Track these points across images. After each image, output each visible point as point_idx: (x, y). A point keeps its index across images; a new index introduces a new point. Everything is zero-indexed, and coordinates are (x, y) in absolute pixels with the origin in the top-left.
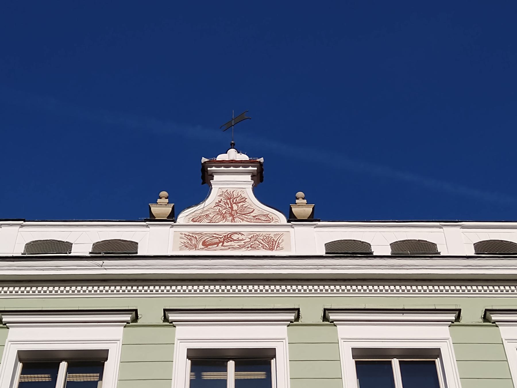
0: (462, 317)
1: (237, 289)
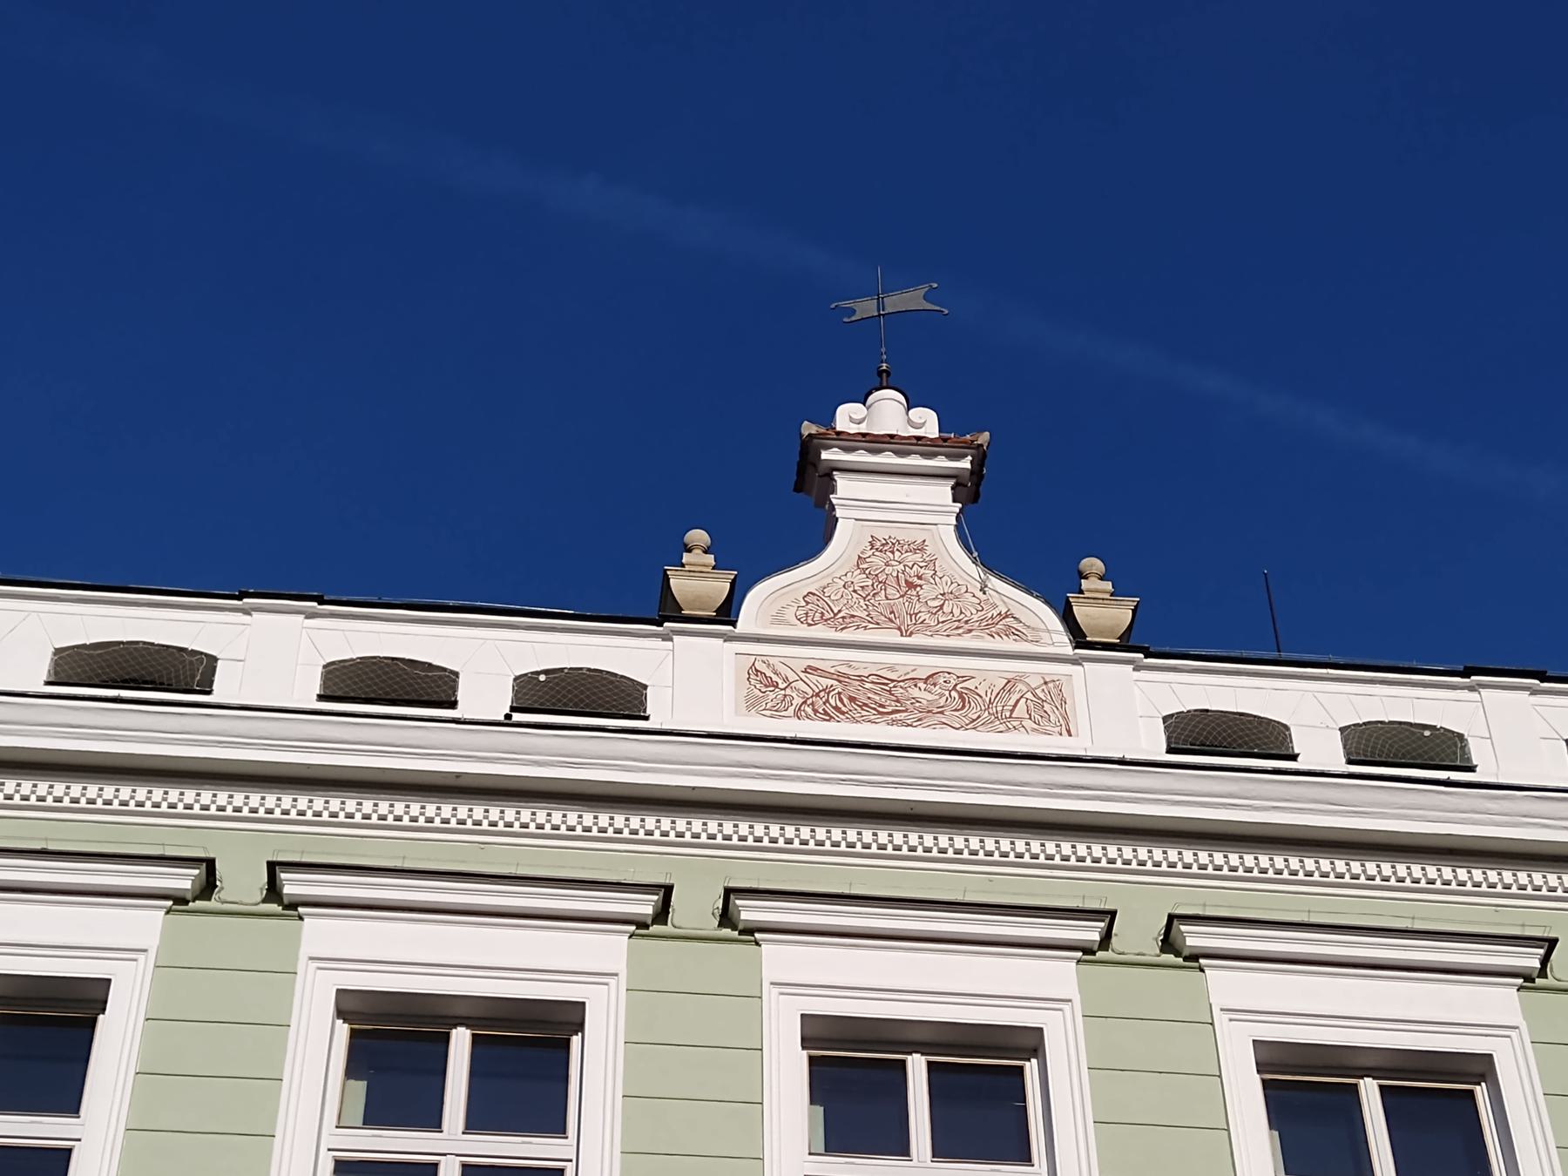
0: (673, 910)
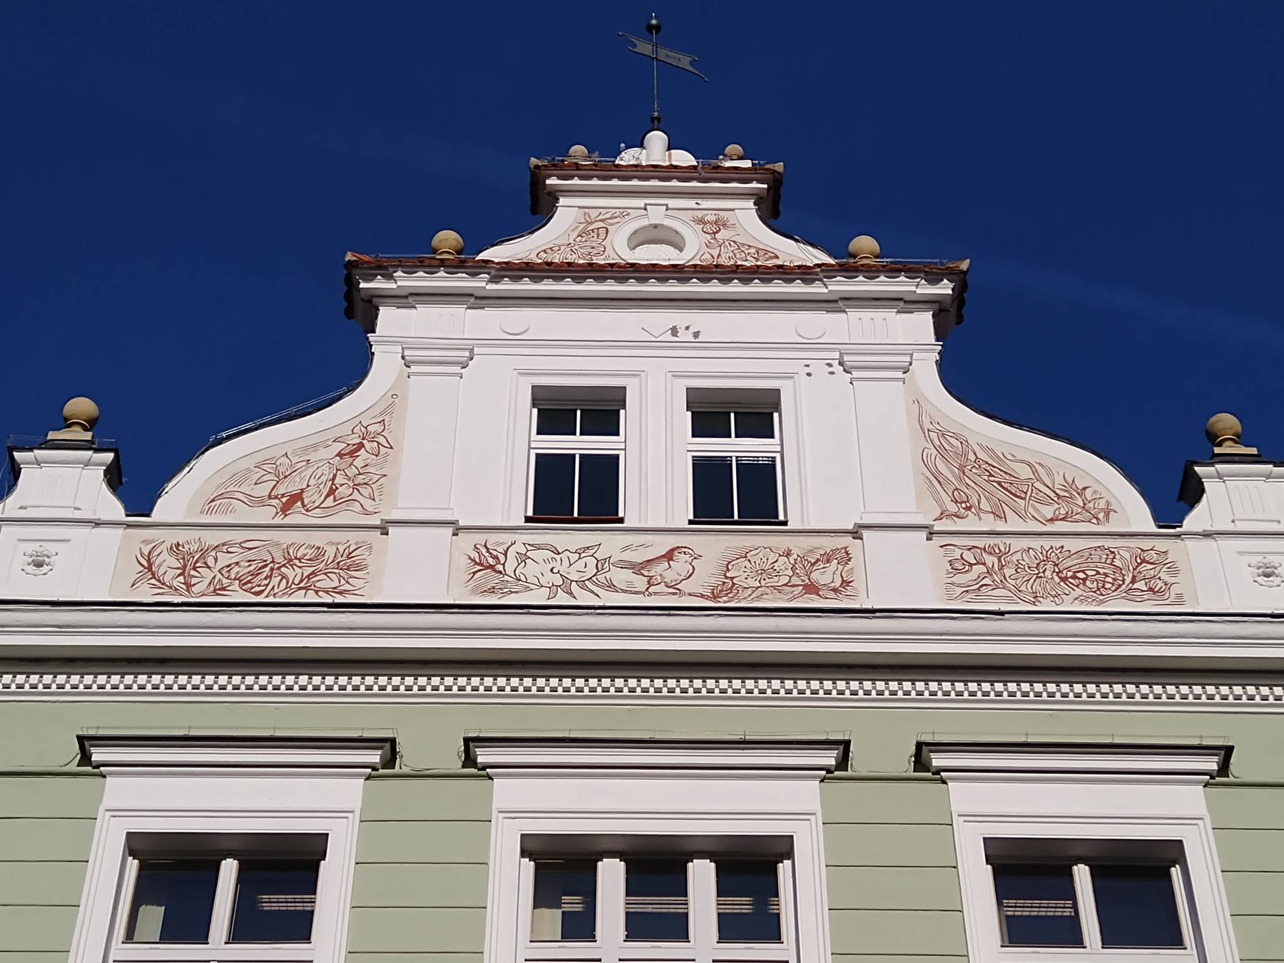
1: (732, 687)
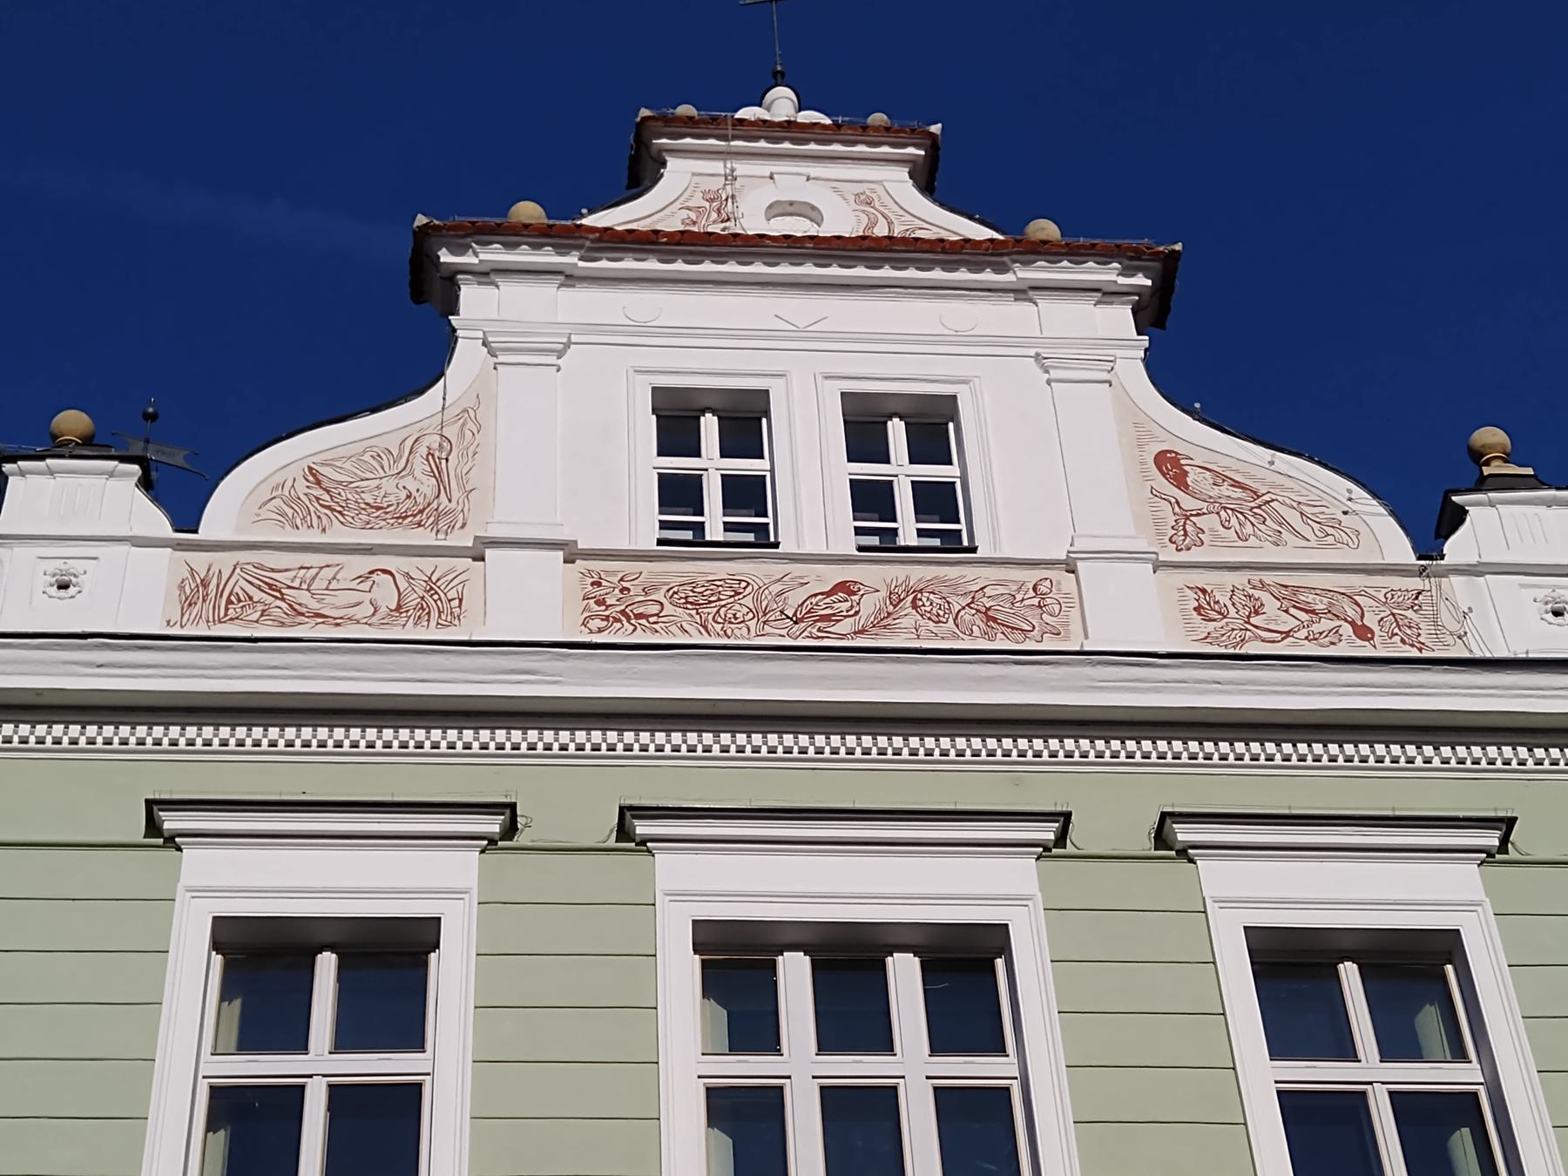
1: (622, 742)
